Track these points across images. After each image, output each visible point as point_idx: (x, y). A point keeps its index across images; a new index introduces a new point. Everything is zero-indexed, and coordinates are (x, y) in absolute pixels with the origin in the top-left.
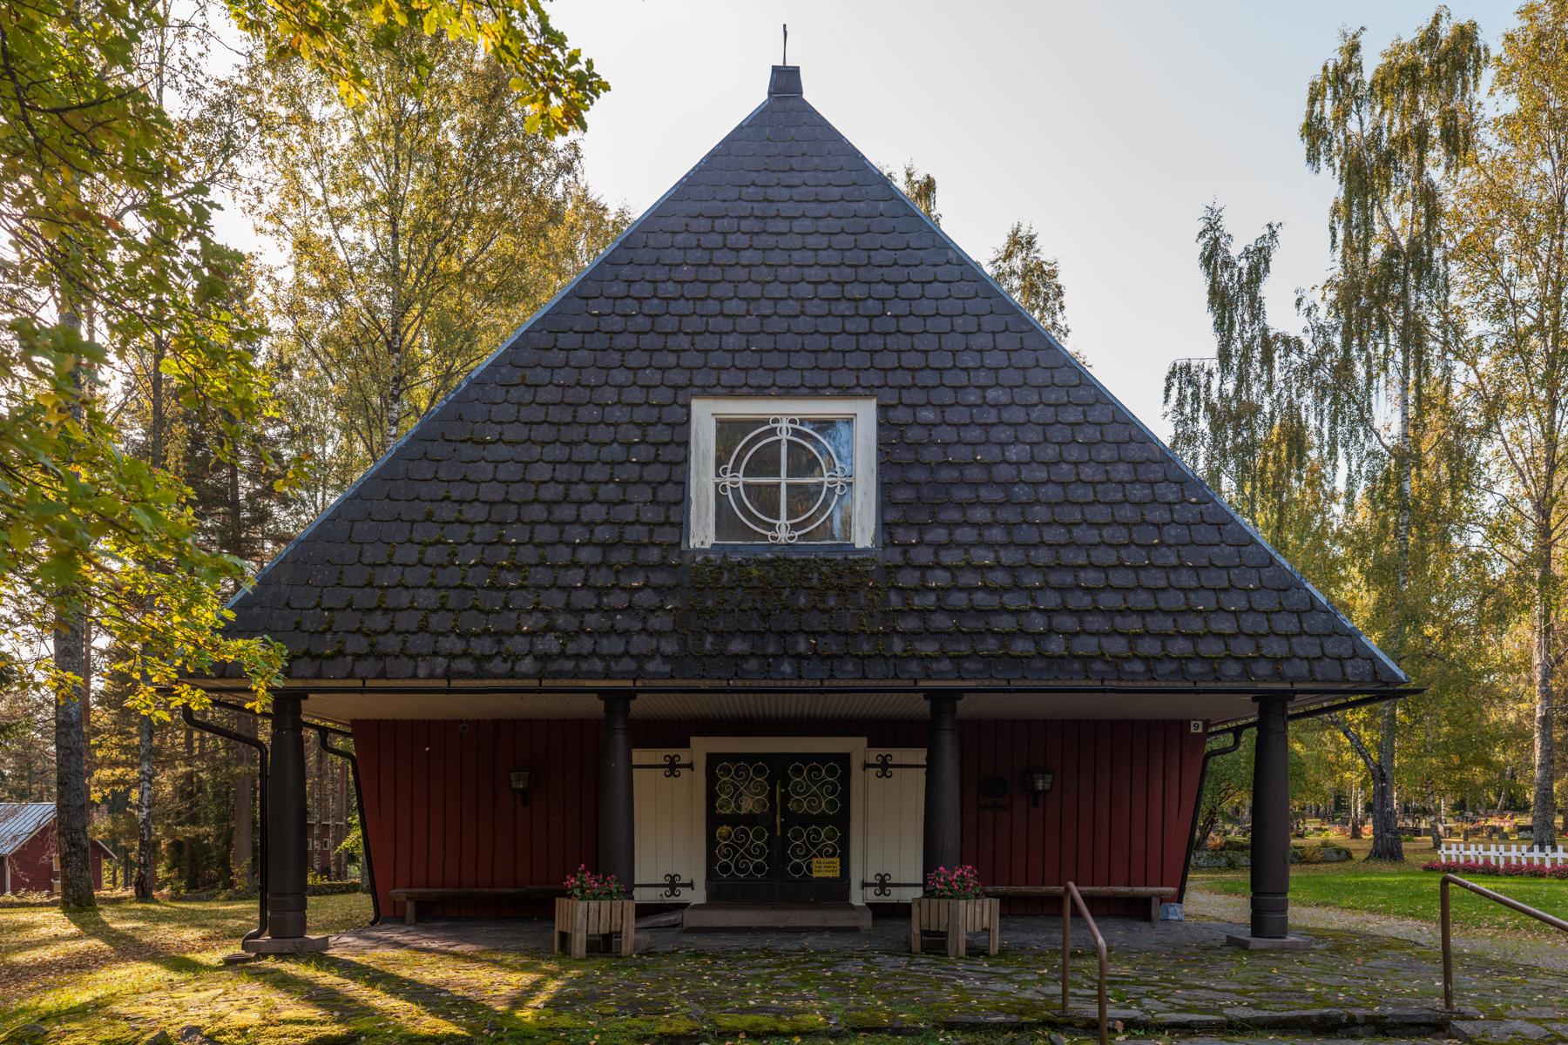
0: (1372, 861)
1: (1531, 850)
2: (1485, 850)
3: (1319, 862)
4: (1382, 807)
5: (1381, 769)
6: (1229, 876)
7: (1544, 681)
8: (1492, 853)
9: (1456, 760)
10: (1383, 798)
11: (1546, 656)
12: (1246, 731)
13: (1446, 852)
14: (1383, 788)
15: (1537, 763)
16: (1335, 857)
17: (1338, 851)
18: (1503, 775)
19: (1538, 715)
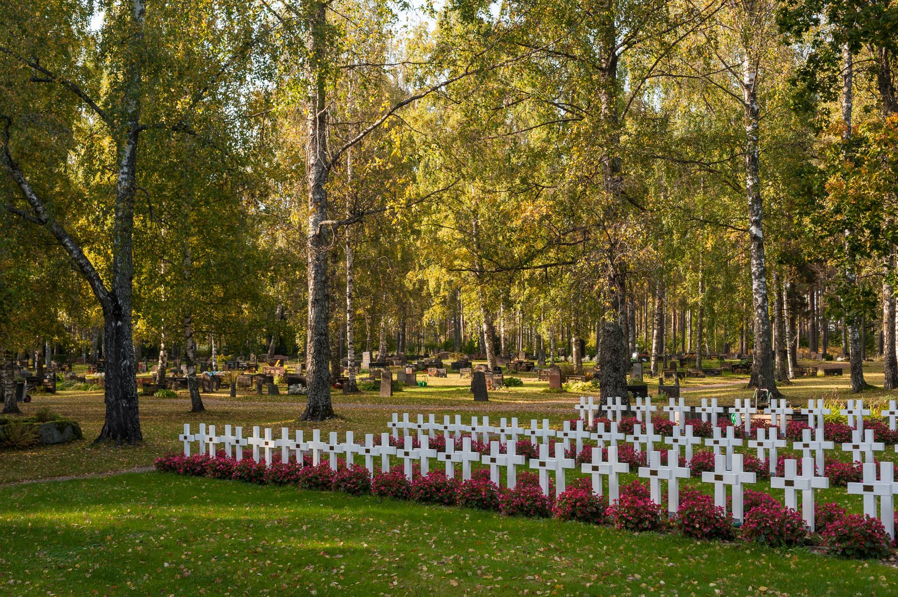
0: (103, 446)
1: (308, 437)
2: (217, 434)
3: (31, 446)
4: (117, 359)
5: (114, 299)
6: (446, 510)
7: (318, 187)
8: (255, 440)
9: (218, 291)
10: (119, 345)
11: (322, 154)
12: (800, 362)
13: (192, 438)
14: (118, 329)
15: (311, 298)
16: (56, 435)
17: (61, 427)
18: (272, 314)
19: (312, 233)
